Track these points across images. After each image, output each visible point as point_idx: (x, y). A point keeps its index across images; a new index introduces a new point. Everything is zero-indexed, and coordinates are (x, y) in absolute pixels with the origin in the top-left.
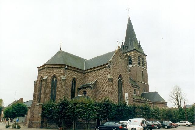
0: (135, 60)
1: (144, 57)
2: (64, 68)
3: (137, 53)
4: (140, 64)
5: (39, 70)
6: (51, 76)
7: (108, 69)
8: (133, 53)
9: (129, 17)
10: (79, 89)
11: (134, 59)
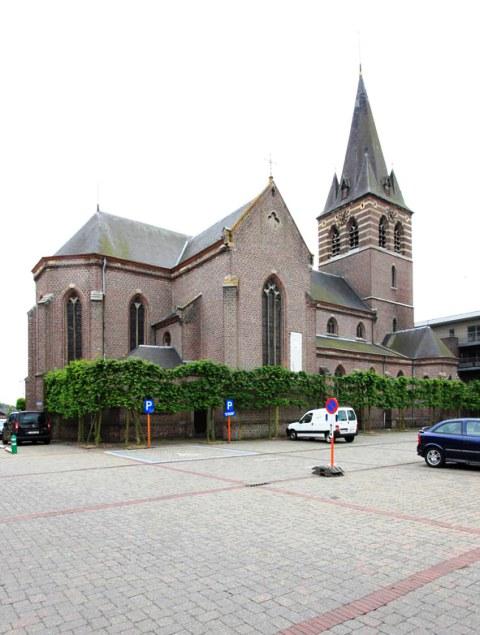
0: (369, 232)
1: (404, 220)
2: (96, 264)
3: (375, 204)
4: (386, 244)
5: (36, 279)
6: (64, 292)
7: (224, 259)
8: (362, 206)
9: (361, 77)
10: (155, 327)
11: (362, 222)
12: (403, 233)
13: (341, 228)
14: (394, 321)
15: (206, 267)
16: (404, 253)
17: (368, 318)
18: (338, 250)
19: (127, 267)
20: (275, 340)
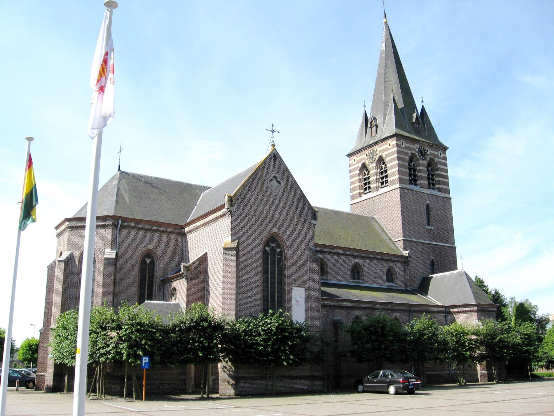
4: (419, 182)
12: (438, 170)
13: (371, 166)
14: (432, 262)
15: (212, 226)
16: (439, 190)
17: (399, 262)
18: (369, 188)
19: (140, 226)
20: (276, 295)
